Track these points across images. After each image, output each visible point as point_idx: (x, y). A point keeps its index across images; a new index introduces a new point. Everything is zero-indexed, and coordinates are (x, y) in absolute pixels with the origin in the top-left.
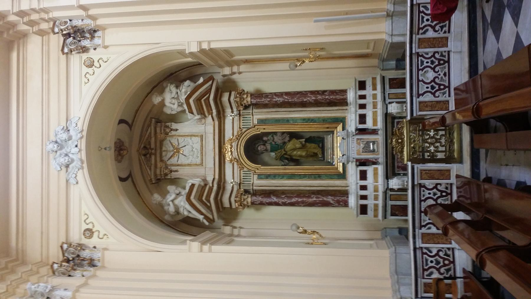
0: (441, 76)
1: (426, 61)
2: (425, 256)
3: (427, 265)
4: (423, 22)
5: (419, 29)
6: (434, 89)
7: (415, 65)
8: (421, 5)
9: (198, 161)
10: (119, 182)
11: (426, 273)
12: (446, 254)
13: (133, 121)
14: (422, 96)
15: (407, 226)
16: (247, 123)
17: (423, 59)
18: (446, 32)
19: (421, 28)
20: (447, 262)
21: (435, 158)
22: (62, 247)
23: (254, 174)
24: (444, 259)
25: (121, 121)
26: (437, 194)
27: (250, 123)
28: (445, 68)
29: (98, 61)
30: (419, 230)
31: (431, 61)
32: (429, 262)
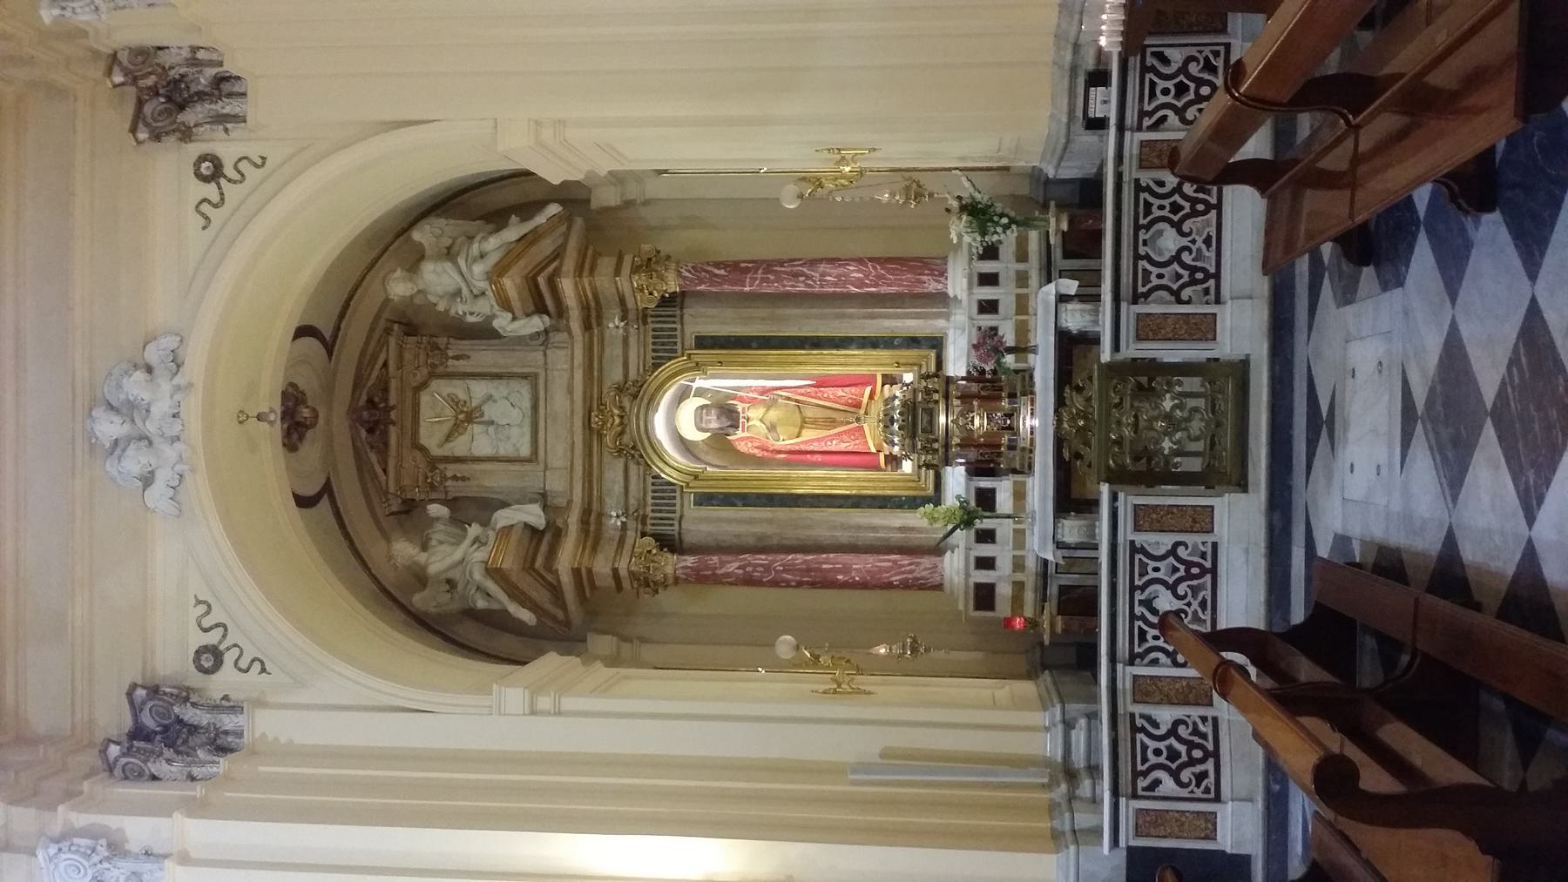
0: (1197, 246)
1: (1157, 202)
2: (1140, 736)
3: (1144, 760)
4: (1152, 95)
5: (1143, 114)
6: (1180, 211)
7: (1125, 557)
8: (1149, 50)
9: (525, 451)
10: (296, 509)
11: (1142, 783)
12: (1196, 732)
13: (337, 329)
14: (1145, 778)
15: (1097, 329)
16: (663, 498)
17: (1151, 199)
18: (1210, 789)
19: (1139, 653)
20: (1197, 754)
21: (1173, 470)
22: (130, 694)
24: (1191, 746)
25: (303, 332)
26: (1173, 565)
30: (1129, 304)
31: (1170, 204)
32: (1150, 754)
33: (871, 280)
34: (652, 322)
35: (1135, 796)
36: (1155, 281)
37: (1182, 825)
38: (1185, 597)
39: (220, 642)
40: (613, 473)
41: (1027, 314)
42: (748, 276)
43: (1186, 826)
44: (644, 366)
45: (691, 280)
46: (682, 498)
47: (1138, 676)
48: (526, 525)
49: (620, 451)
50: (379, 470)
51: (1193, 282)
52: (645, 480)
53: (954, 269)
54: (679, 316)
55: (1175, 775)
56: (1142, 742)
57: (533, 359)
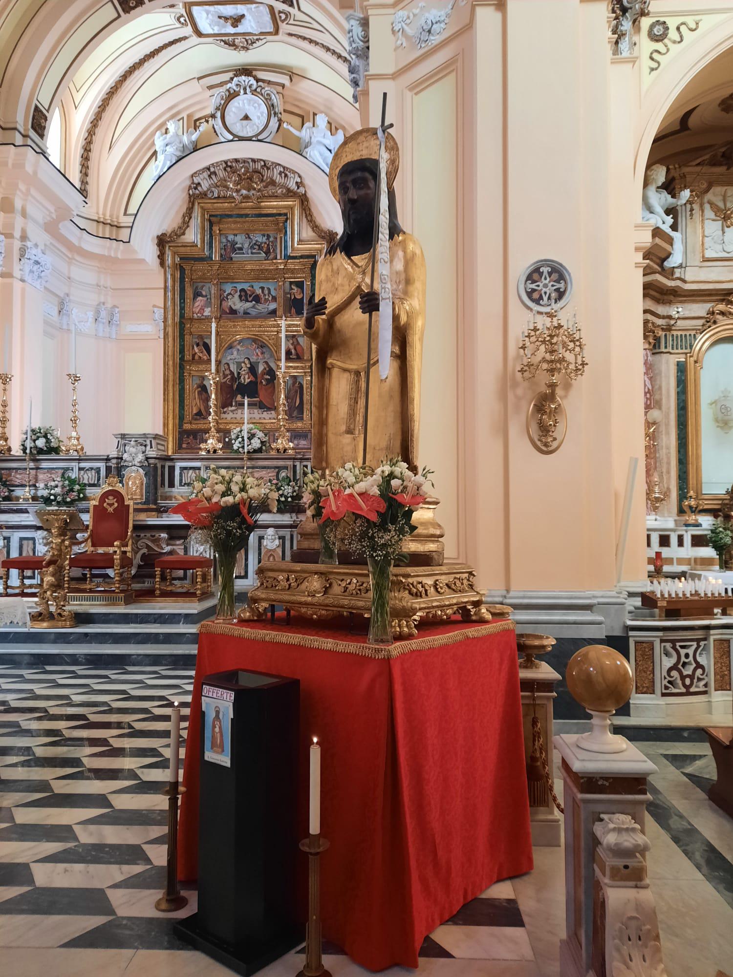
11: (668, 645)
23: (686, 354)
24: (692, 677)
27: (666, 347)
29: (678, 29)
37: (644, 672)
39: (670, 39)
40: (700, 309)
43: (644, 674)
48: (669, 255)
49: (713, 313)
50: (698, 161)
55: (674, 667)
56: (692, 645)
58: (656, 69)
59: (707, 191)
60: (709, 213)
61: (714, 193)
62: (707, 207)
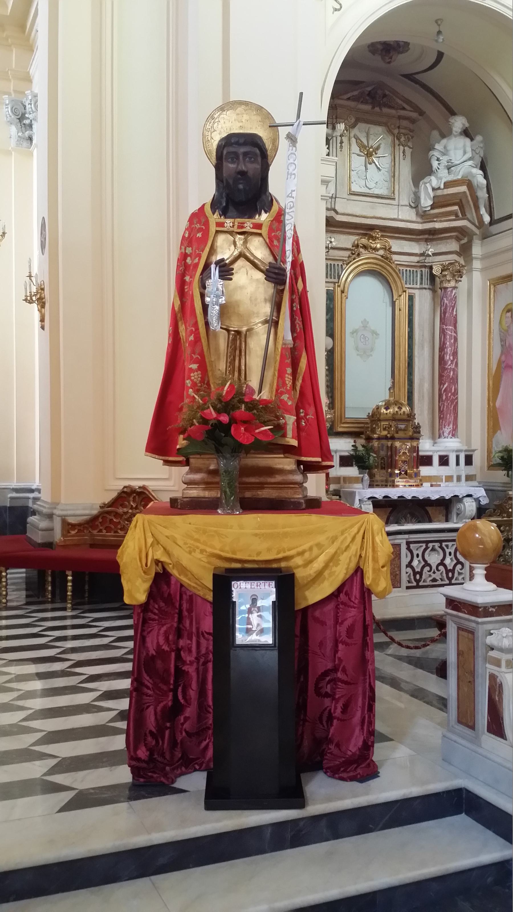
28: (442, 580)
33: (450, 397)
34: (422, 271)
35: (408, 543)
36: (415, 553)
38: (438, 570)
41: (446, 481)
42: (453, 328)
44: (399, 264)
45: (451, 295)
46: (331, 282)
47: (400, 546)
49: (357, 246)
50: (349, 95)
51: (447, 571)
52: (341, 260)
53: (458, 442)
54: (421, 286)
57: (405, 198)
58: (339, 10)
59: (353, 126)
60: (355, 148)
61: (359, 129)
62: (353, 140)
